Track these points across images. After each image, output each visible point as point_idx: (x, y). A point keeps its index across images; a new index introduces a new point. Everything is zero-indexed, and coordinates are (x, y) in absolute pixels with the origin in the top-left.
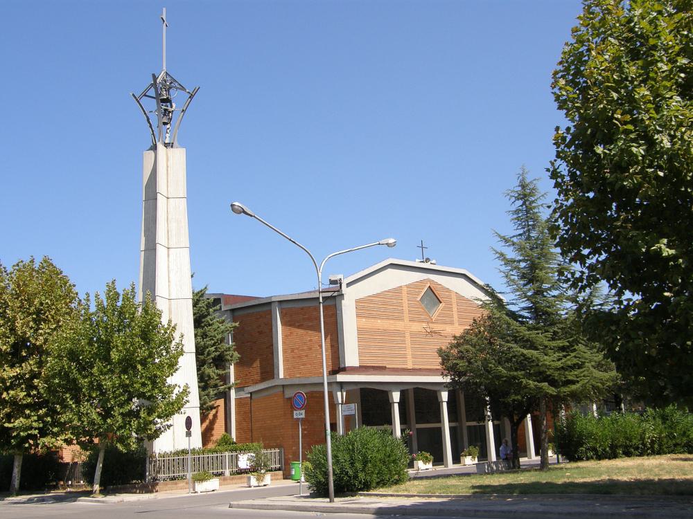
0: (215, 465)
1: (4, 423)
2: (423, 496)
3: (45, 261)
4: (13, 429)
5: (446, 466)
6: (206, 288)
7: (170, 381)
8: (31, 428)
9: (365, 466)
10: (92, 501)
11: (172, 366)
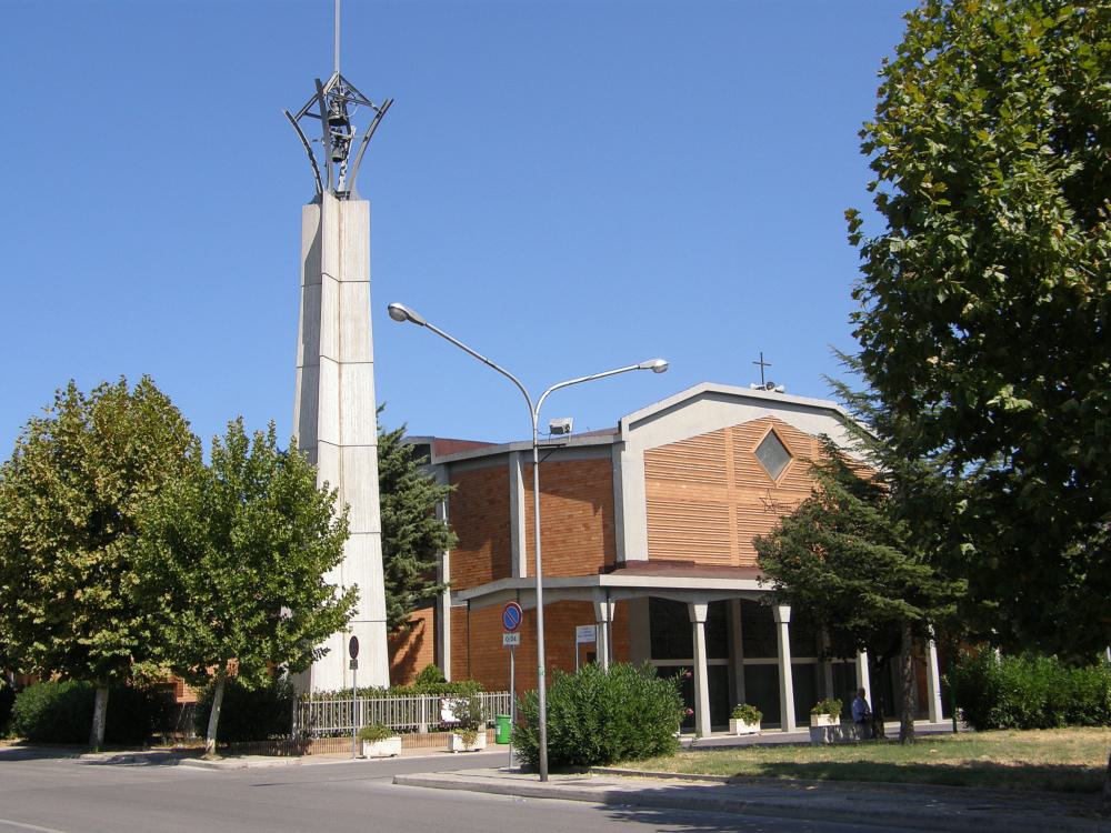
0: (404, 715)
1: (79, 637)
2: (686, 778)
3: (145, 384)
4: (89, 648)
5: (785, 729)
6: (403, 428)
7: (329, 578)
8: (119, 646)
9: (603, 724)
10: (200, 765)
11: (332, 555)
